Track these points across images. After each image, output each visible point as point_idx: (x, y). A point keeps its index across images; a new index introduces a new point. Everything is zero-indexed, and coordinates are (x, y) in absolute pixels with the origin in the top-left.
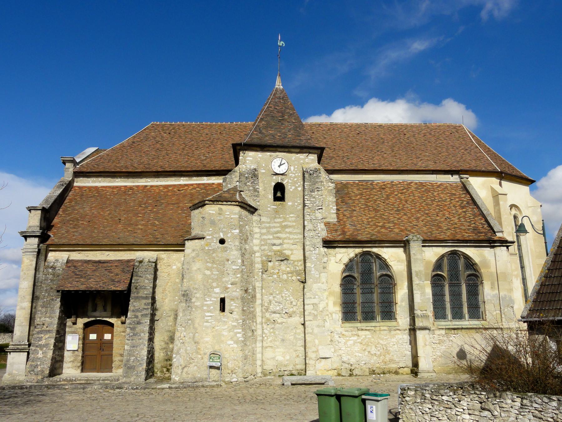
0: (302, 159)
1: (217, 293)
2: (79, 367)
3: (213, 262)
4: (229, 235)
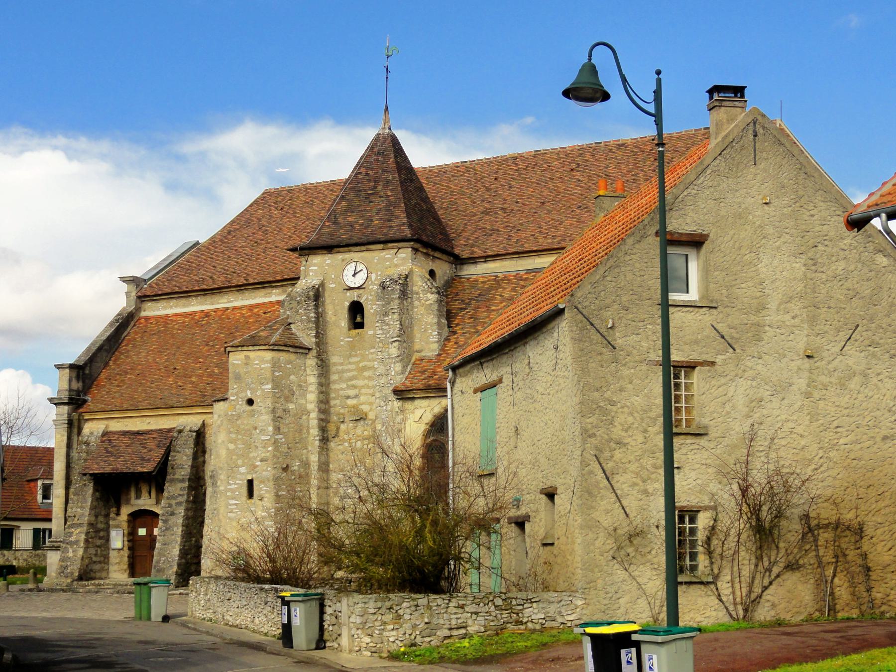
0: (388, 260)
1: (243, 474)
2: (125, 570)
3: (238, 432)
4: (259, 393)
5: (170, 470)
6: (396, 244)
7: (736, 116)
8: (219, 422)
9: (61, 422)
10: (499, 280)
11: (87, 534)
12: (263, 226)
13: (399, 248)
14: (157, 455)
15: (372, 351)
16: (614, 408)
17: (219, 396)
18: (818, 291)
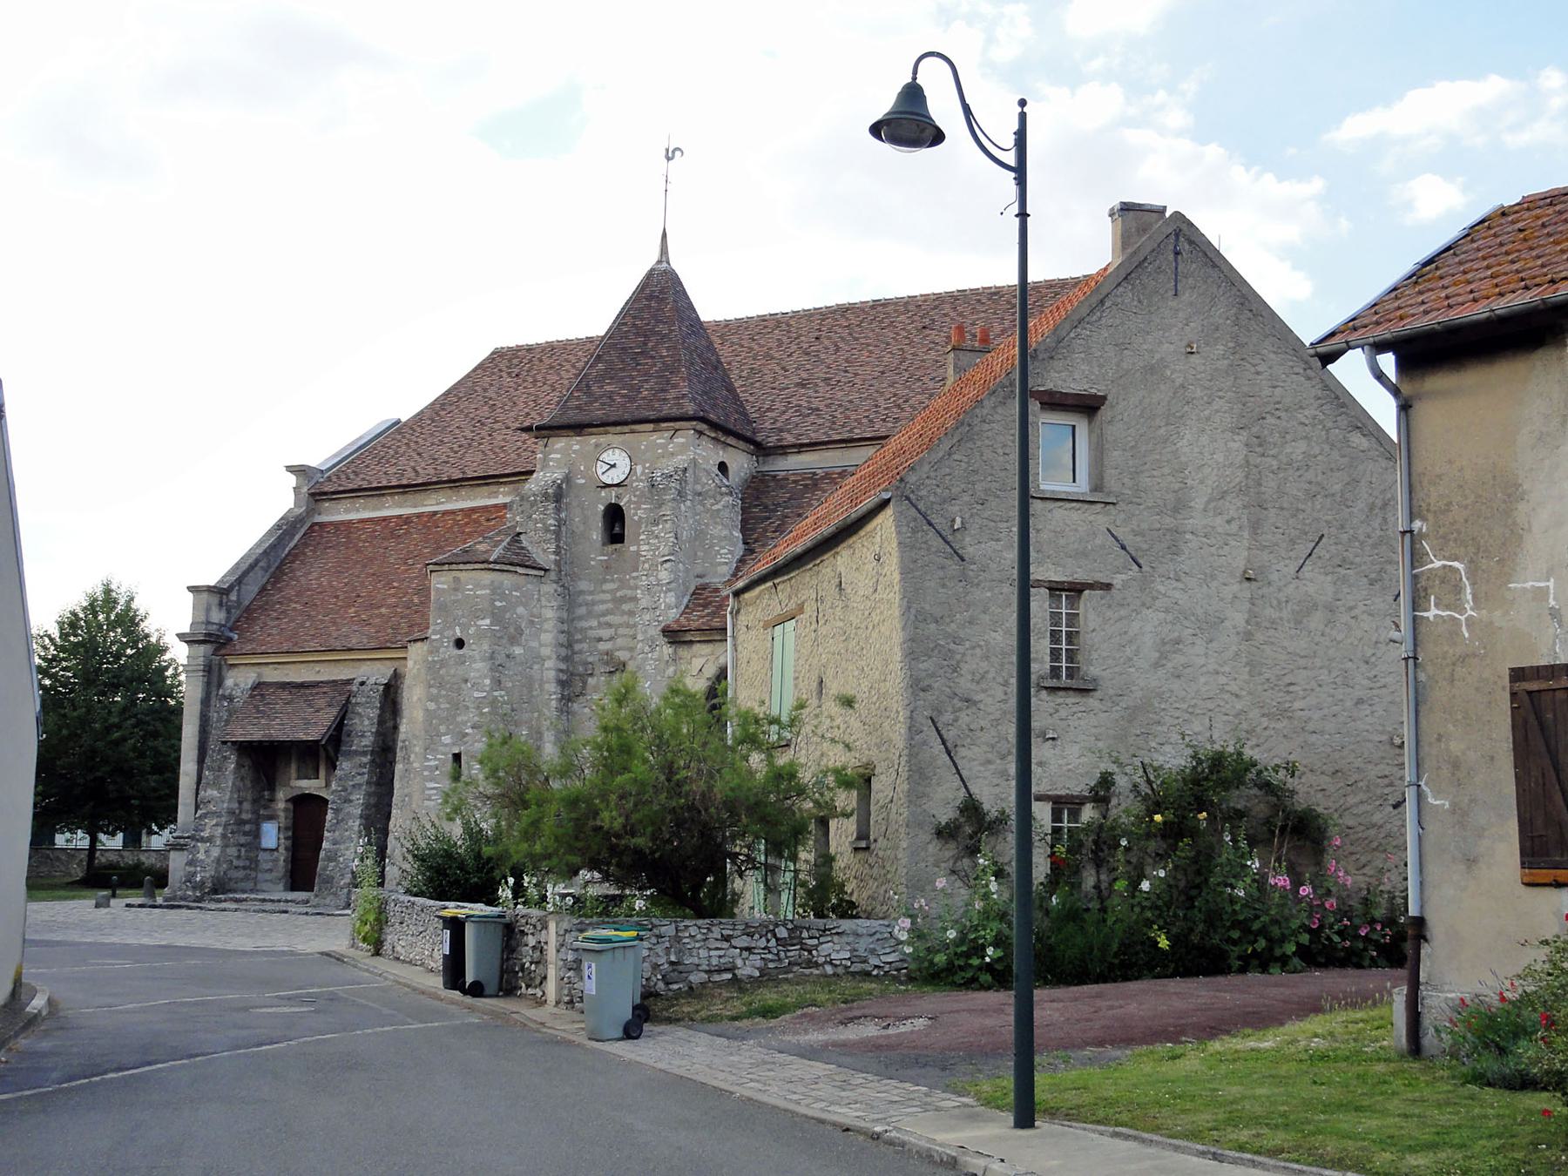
1: (446, 745)
3: (441, 686)
5: (344, 738)
6: (672, 424)
7: (1151, 224)
8: (415, 671)
9: (195, 668)
10: (817, 480)
11: (226, 826)
12: (491, 399)
13: (677, 430)
14: (327, 717)
15: (635, 574)
16: (961, 649)
17: (417, 635)
18: (1265, 484)
